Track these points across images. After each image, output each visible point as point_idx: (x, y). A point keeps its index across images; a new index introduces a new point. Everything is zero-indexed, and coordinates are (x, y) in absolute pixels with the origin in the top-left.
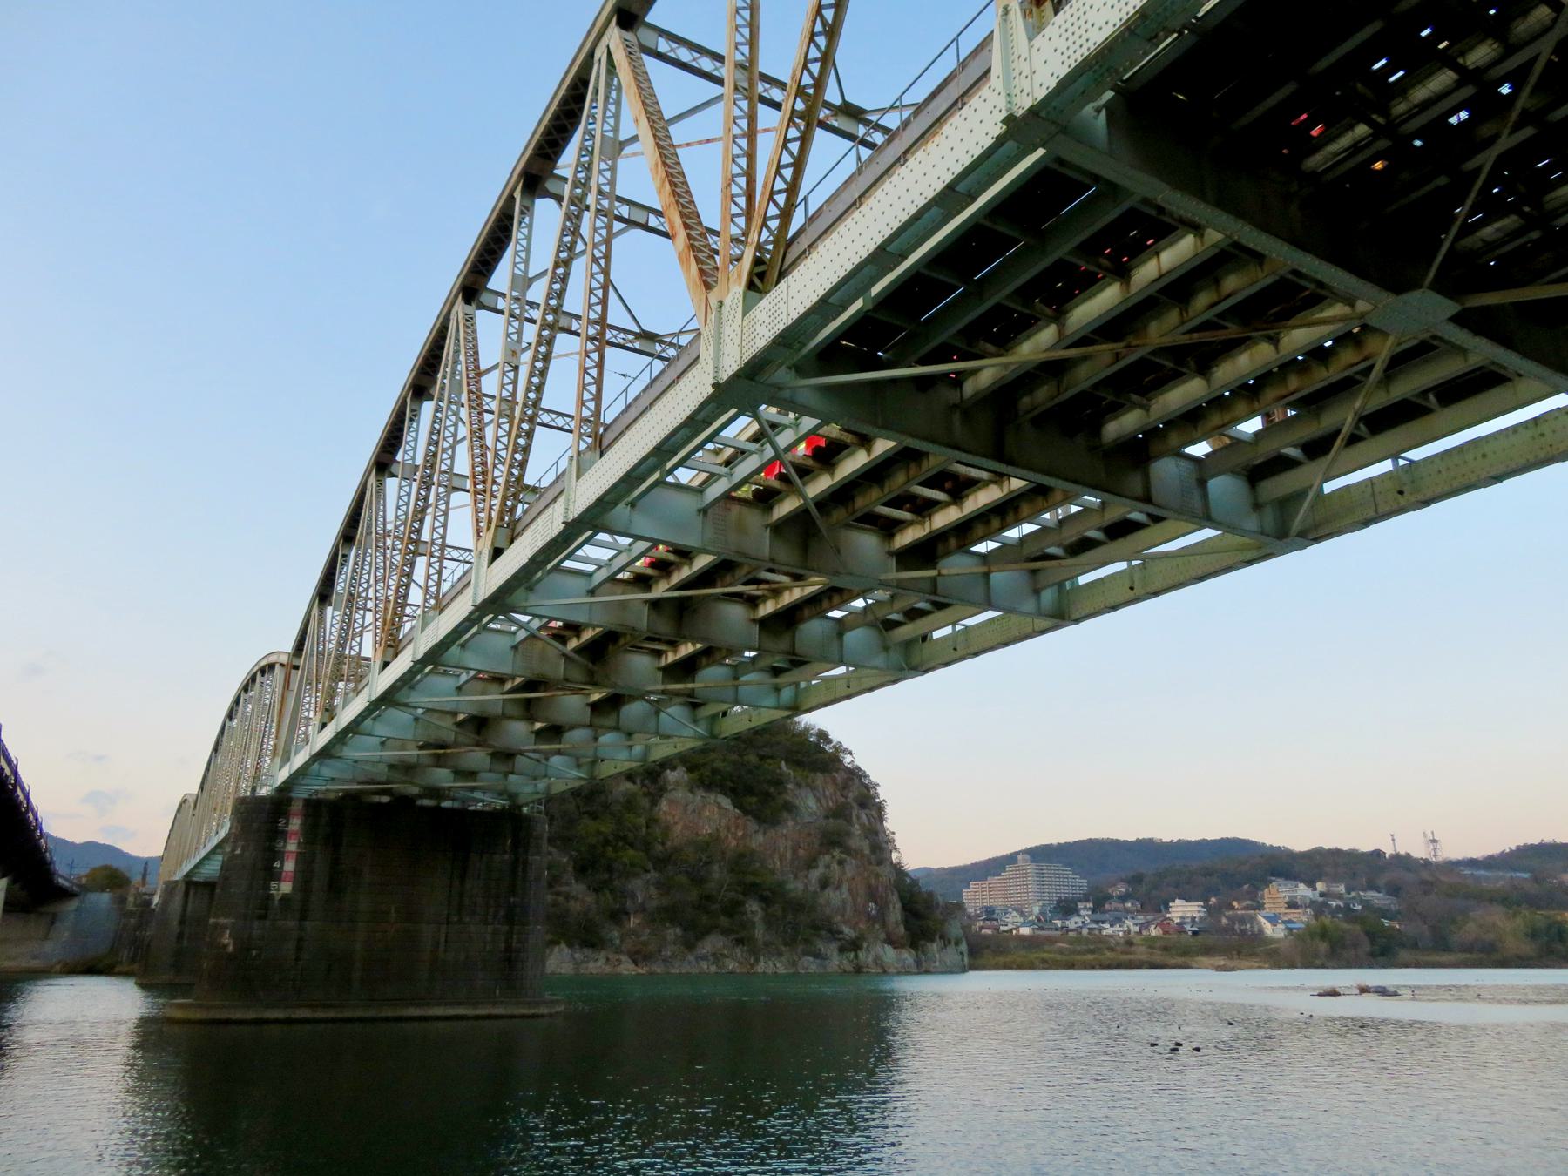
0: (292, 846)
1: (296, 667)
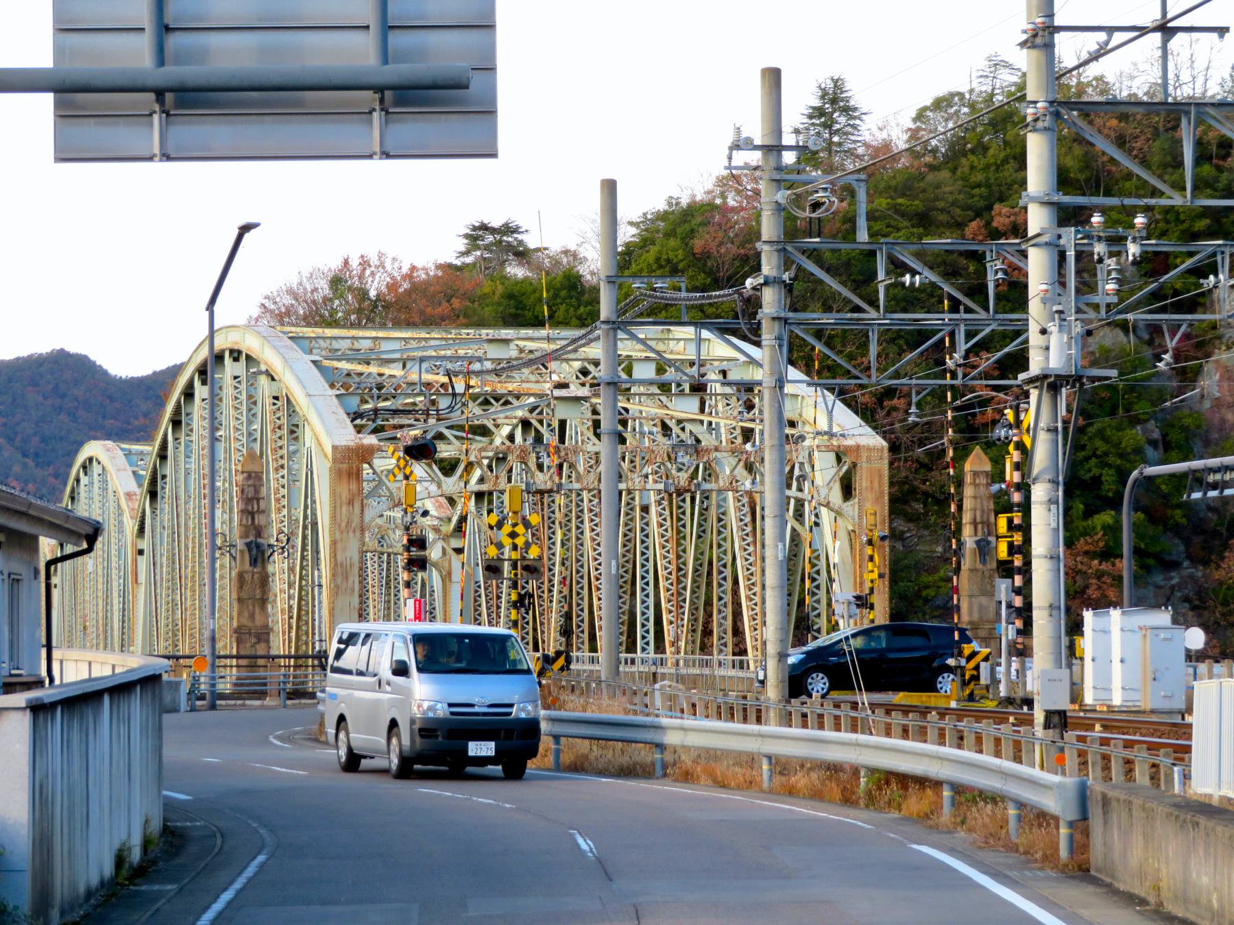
1: (141, 552)
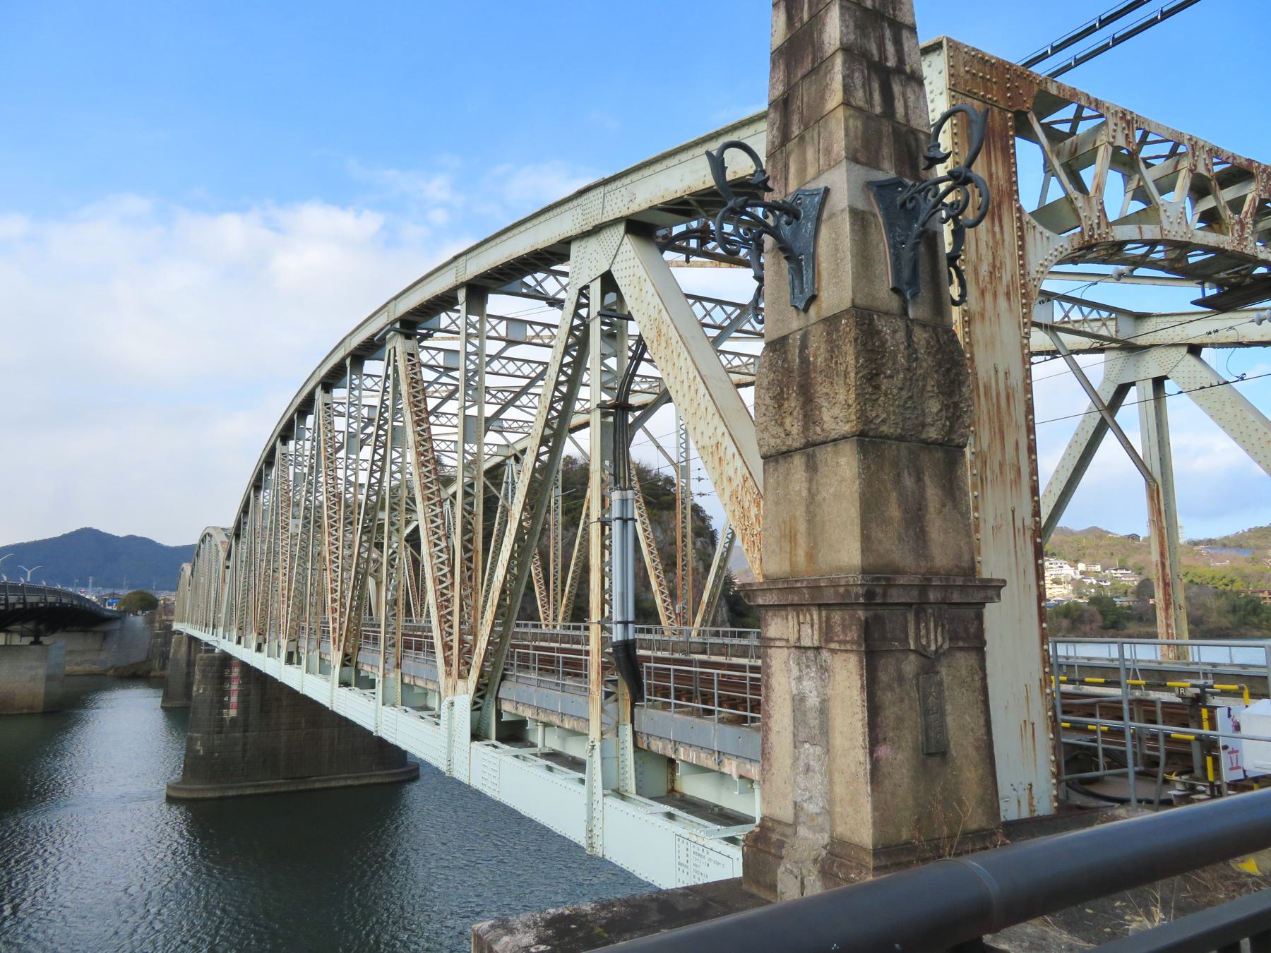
0: (234, 686)
1: (228, 567)
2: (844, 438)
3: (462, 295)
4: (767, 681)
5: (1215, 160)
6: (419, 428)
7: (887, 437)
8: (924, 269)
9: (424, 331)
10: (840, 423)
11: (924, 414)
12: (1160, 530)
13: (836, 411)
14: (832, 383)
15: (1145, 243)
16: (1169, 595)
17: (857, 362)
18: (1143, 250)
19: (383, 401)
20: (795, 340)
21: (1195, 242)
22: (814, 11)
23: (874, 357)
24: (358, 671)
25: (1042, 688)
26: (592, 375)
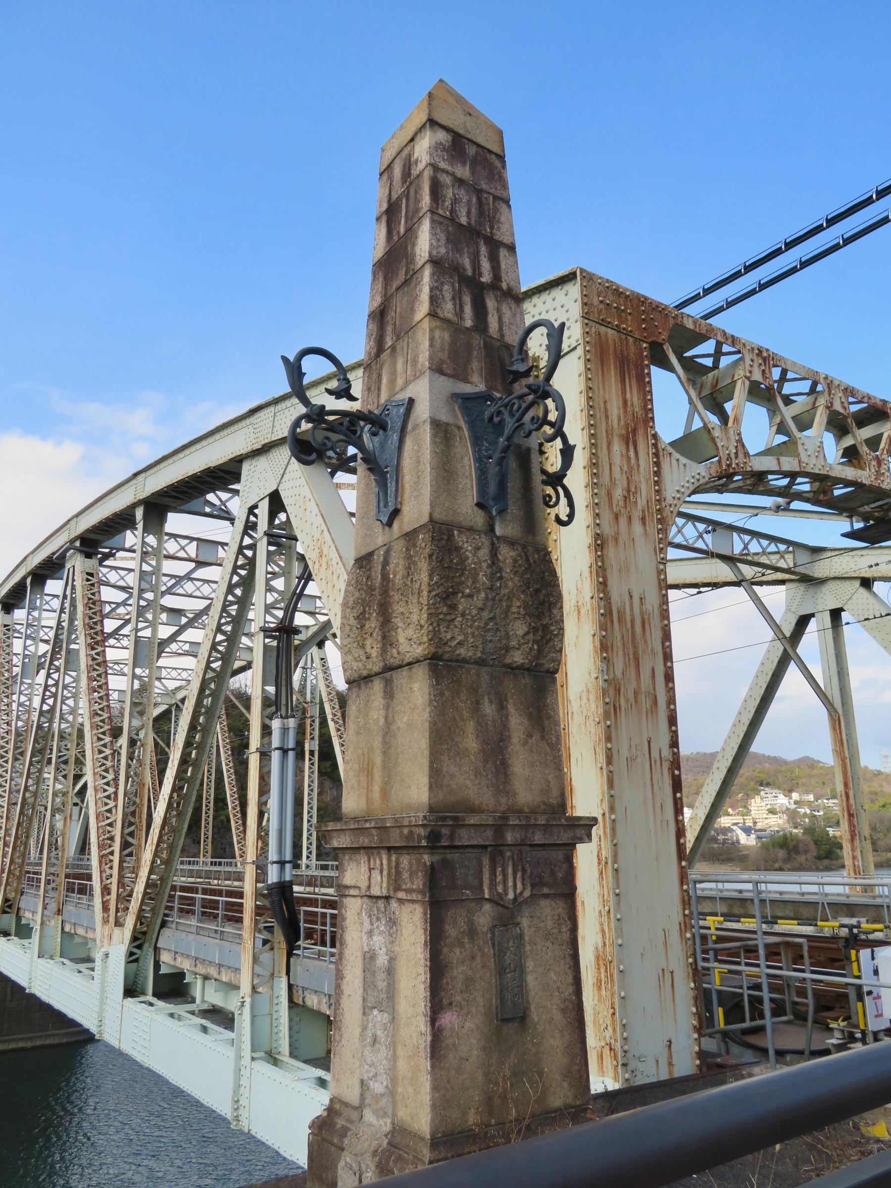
2: (418, 661)
3: (139, 513)
4: (342, 935)
5: (851, 399)
6: (93, 652)
7: (465, 661)
8: (514, 485)
9: (107, 550)
10: (415, 646)
11: (508, 637)
12: (843, 760)
13: (410, 632)
14: (407, 602)
15: (785, 474)
16: (854, 826)
17: (431, 579)
18: (785, 482)
19: (59, 623)
20: (378, 558)
21: (833, 475)
22: (410, 224)
23: (451, 575)
24: (19, 918)
25: (682, 933)
26: (260, 597)
